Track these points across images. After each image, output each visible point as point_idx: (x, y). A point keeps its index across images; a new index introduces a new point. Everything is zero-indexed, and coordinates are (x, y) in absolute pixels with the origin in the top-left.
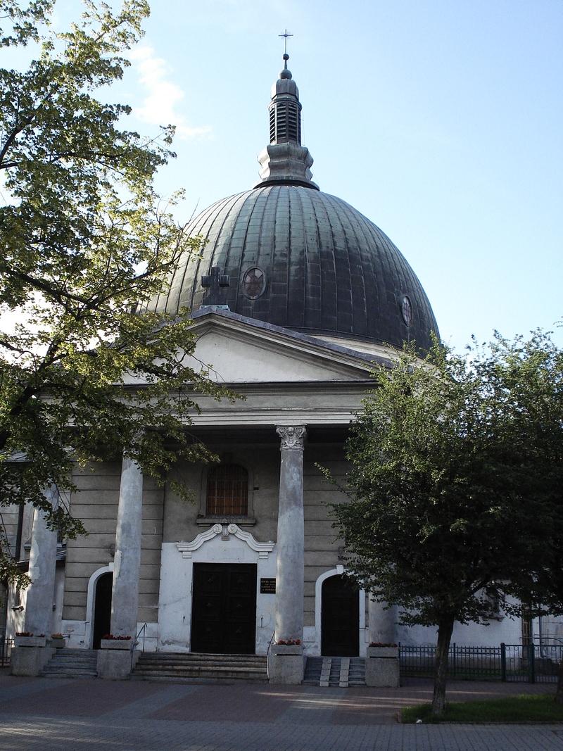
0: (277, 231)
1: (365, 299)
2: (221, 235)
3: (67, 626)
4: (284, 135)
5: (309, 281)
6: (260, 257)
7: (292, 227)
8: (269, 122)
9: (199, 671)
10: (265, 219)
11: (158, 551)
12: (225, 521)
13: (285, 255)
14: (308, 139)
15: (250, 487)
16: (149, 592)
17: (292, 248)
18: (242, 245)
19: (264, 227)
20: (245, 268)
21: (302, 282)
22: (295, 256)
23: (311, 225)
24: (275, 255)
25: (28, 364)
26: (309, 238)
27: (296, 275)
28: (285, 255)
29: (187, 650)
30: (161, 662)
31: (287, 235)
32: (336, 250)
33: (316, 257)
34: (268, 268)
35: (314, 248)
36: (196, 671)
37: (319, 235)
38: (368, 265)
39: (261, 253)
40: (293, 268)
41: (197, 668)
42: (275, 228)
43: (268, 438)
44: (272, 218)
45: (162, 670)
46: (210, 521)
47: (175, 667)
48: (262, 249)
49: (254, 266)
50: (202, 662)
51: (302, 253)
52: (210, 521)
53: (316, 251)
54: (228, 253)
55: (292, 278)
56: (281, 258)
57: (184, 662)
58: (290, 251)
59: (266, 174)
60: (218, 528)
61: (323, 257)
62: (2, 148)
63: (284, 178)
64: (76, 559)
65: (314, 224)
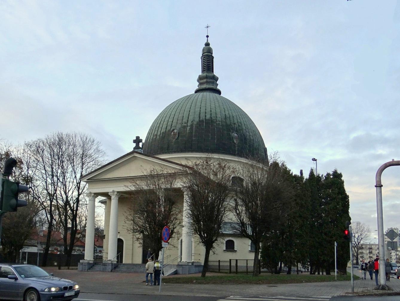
1: (216, 137)
4: (206, 70)
5: (194, 132)
6: (177, 125)
7: (190, 112)
8: (201, 65)
13: (185, 123)
14: (217, 72)
17: (189, 120)
21: (191, 133)
22: (189, 124)
24: (183, 123)
25: (99, 196)
27: (189, 130)
32: (205, 119)
33: (197, 123)
35: (197, 119)
37: (200, 113)
38: (219, 124)
39: (178, 123)
40: (188, 128)
42: (184, 113)
44: (184, 109)
49: (175, 128)
55: (187, 132)
58: (188, 121)
61: (201, 122)
62: (238, 297)
63: (204, 88)
65: (199, 109)
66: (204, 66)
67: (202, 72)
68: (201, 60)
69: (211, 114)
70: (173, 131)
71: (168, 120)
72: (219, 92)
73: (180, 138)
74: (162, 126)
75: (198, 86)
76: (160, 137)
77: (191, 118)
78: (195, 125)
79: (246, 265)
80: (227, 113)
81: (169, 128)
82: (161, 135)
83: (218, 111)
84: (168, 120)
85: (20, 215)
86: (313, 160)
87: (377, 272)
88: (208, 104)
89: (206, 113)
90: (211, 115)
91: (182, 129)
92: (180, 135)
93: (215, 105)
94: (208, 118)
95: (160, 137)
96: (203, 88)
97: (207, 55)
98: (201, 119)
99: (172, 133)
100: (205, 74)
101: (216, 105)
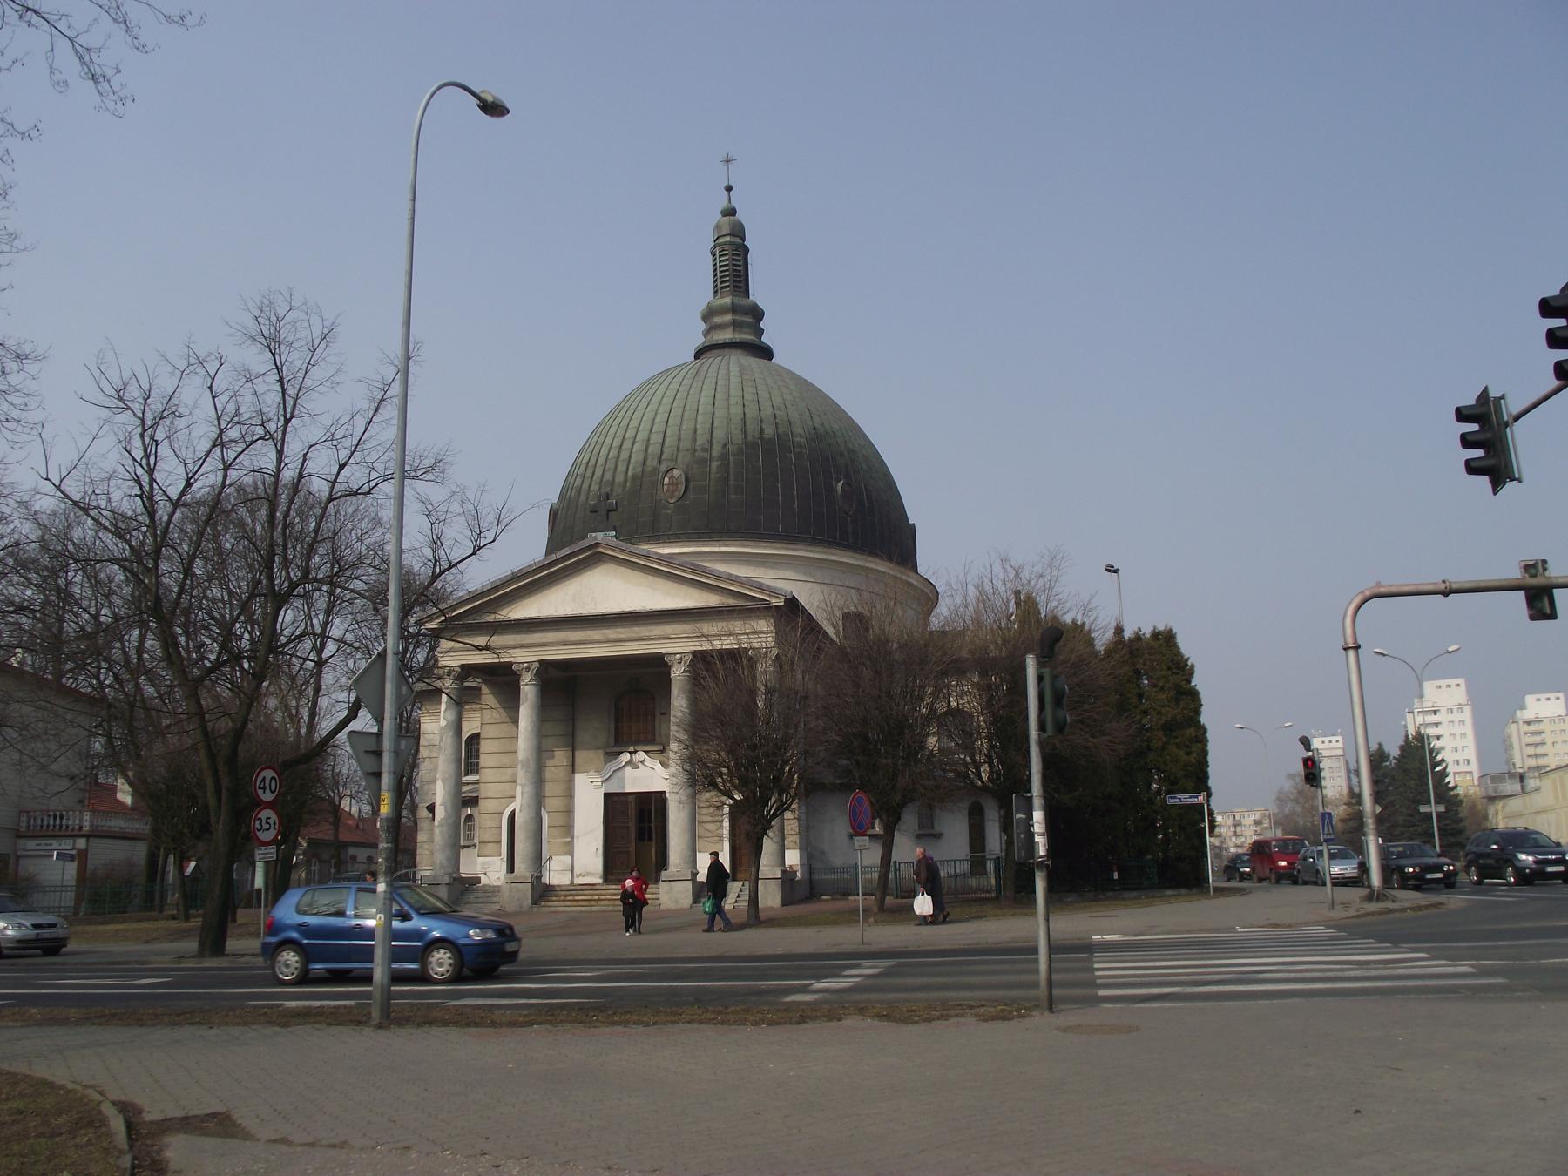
0: (698, 422)
1: (795, 493)
2: (641, 428)
3: (484, 863)
5: (732, 477)
9: (599, 900)
10: (688, 407)
11: (571, 781)
12: (632, 749)
15: (657, 713)
16: (564, 824)
17: (714, 440)
18: (661, 440)
19: (686, 417)
20: (663, 468)
22: (717, 450)
23: (736, 410)
24: (695, 450)
26: (733, 427)
27: (717, 473)
28: (706, 450)
29: (600, 881)
30: (563, 893)
31: (709, 426)
34: (687, 466)
35: (738, 438)
36: (595, 900)
40: (715, 464)
41: (596, 897)
42: (696, 420)
43: (658, 664)
45: (563, 901)
46: (618, 749)
47: (577, 898)
48: (682, 444)
49: (672, 464)
50: (603, 892)
51: (725, 446)
52: (618, 749)
53: (740, 442)
54: (646, 450)
55: (713, 476)
56: (702, 454)
57: (586, 892)
59: (699, 341)
60: (625, 757)
61: (749, 447)
63: (727, 341)
64: (490, 795)
65: (740, 408)
66: (723, 274)
67: (716, 292)
68: (710, 258)
69: (777, 424)
70: (669, 474)
71: (646, 438)
72: (766, 353)
73: (691, 496)
74: (630, 457)
75: (706, 334)
76: (627, 489)
77: (719, 434)
78: (734, 455)
79: (577, 753)
80: (817, 420)
81: (652, 463)
82: (628, 484)
83: (794, 415)
84: (649, 440)
85: (284, 743)
86: (1108, 570)
87: (385, 603)
88: (764, 394)
89: (761, 421)
90: (777, 428)
91: (695, 466)
92: (691, 485)
93: (782, 396)
94: (771, 437)
95: (627, 489)
96: (725, 339)
97: (731, 243)
98: (750, 438)
99: (666, 480)
100: (727, 300)
101: (785, 396)
